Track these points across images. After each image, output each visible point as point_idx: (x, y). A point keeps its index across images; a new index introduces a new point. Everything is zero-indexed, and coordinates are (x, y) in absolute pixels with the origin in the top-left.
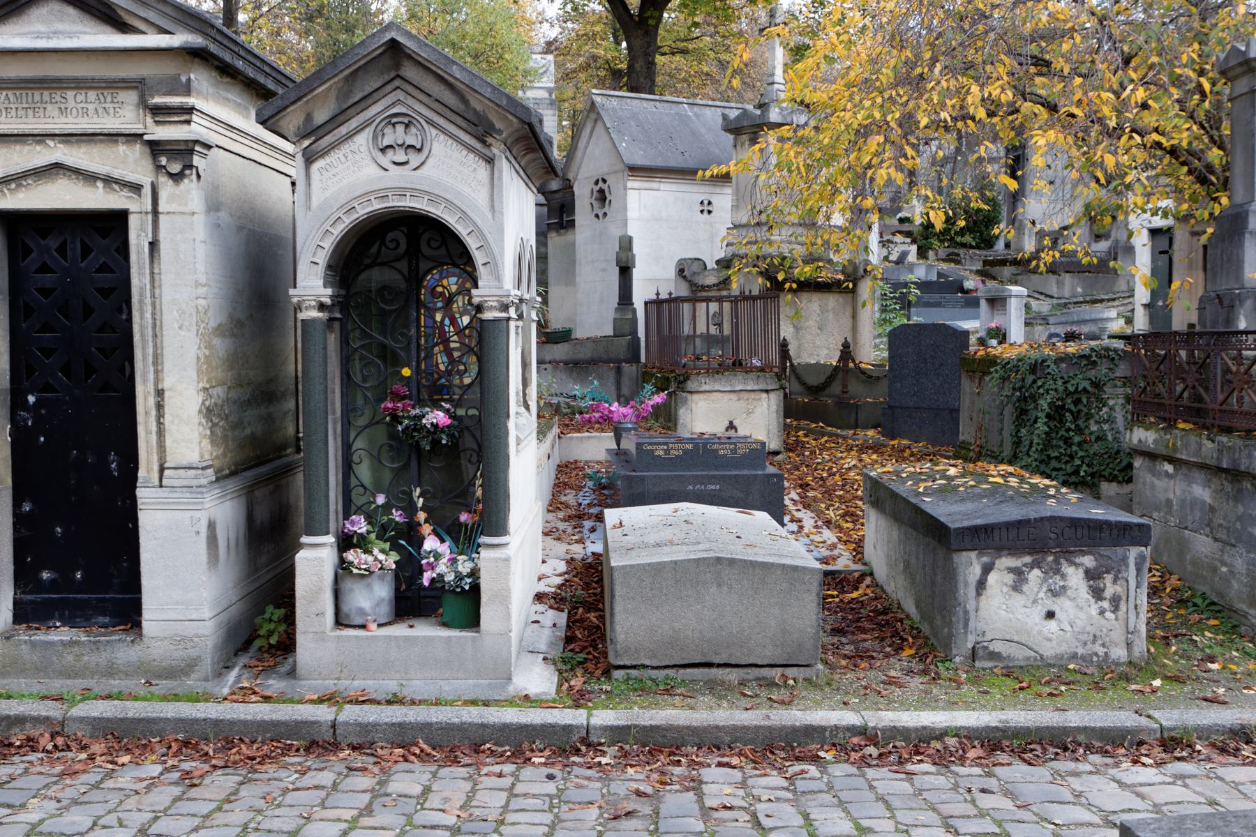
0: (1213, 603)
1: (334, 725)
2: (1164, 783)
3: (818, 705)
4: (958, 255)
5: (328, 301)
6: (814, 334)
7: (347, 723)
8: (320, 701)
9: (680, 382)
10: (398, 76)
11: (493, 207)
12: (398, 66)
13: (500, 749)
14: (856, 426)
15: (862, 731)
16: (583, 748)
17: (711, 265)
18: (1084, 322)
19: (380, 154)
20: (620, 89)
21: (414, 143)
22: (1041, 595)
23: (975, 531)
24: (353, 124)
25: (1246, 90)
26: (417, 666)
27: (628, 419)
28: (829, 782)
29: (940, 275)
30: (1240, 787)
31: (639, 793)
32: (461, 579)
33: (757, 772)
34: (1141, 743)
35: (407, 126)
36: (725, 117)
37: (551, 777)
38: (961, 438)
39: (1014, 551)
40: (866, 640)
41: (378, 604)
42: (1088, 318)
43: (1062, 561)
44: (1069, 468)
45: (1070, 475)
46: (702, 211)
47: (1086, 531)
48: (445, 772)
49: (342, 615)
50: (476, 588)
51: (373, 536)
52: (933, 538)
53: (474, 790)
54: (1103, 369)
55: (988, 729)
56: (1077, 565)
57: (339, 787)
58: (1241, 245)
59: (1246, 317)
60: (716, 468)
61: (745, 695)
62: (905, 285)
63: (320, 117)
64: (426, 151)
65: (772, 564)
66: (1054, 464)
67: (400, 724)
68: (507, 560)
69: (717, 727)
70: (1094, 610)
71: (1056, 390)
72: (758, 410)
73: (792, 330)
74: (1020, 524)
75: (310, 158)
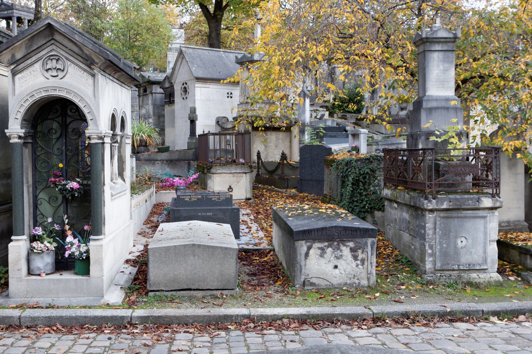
0: (410, 261)
1: (20, 318)
2: (368, 336)
3: (233, 306)
4: (346, 116)
5: (22, 135)
6: (270, 149)
7: (26, 317)
8: (17, 307)
9: (208, 169)
10: (53, 39)
11: (94, 95)
12: (52, 35)
13: (92, 327)
14: (287, 187)
15: (248, 317)
16: (129, 326)
17: (231, 119)
18: (393, 144)
19: (45, 72)
20: (193, 45)
21: (60, 68)
22: (332, 259)
23: (304, 232)
24: (33, 59)
25: (422, 50)
26: (64, 292)
27: (182, 185)
28: (228, 338)
29: (337, 124)
30: (398, 338)
31: (145, 345)
32: (82, 254)
33: (200, 335)
34: (364, 320)
35: (57, 60)
36: (236, 57)
37: (110, 339)
38: (325, 193)
39: (320, 240)
40: (264, 278)
41: (46, 265)
42: (395, 142)
43: (341, 244)
44: (362, 205)
45: (362, 208)
46: (228, 97)
47: (350, 232)
48: (65, 337)
49: (30, 270)
50: (88, 258)
51: (45, 236)
52: (291, 236)
53: (74, 345)
54: (375, 165)
55: (302, 315)
56: (347, 246)
57: (14, 345)
58: (420, 114)
59: (422, 143)
60: (211, 206)
61: (204, 302)
62: (318, 128)
63: (19, 56)
64: (65, 71)
65: (217, 247)
66: (355, 204)
67: (49, 317)
68: (101, 246)
69: (187, 316)
70: (354, 264)
71: (356, 173)
72: (242, 181)
73: (263, 147)
74: (323, 229)
75: (14, 74)
